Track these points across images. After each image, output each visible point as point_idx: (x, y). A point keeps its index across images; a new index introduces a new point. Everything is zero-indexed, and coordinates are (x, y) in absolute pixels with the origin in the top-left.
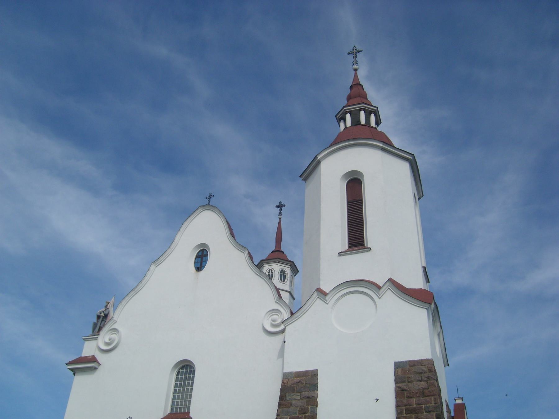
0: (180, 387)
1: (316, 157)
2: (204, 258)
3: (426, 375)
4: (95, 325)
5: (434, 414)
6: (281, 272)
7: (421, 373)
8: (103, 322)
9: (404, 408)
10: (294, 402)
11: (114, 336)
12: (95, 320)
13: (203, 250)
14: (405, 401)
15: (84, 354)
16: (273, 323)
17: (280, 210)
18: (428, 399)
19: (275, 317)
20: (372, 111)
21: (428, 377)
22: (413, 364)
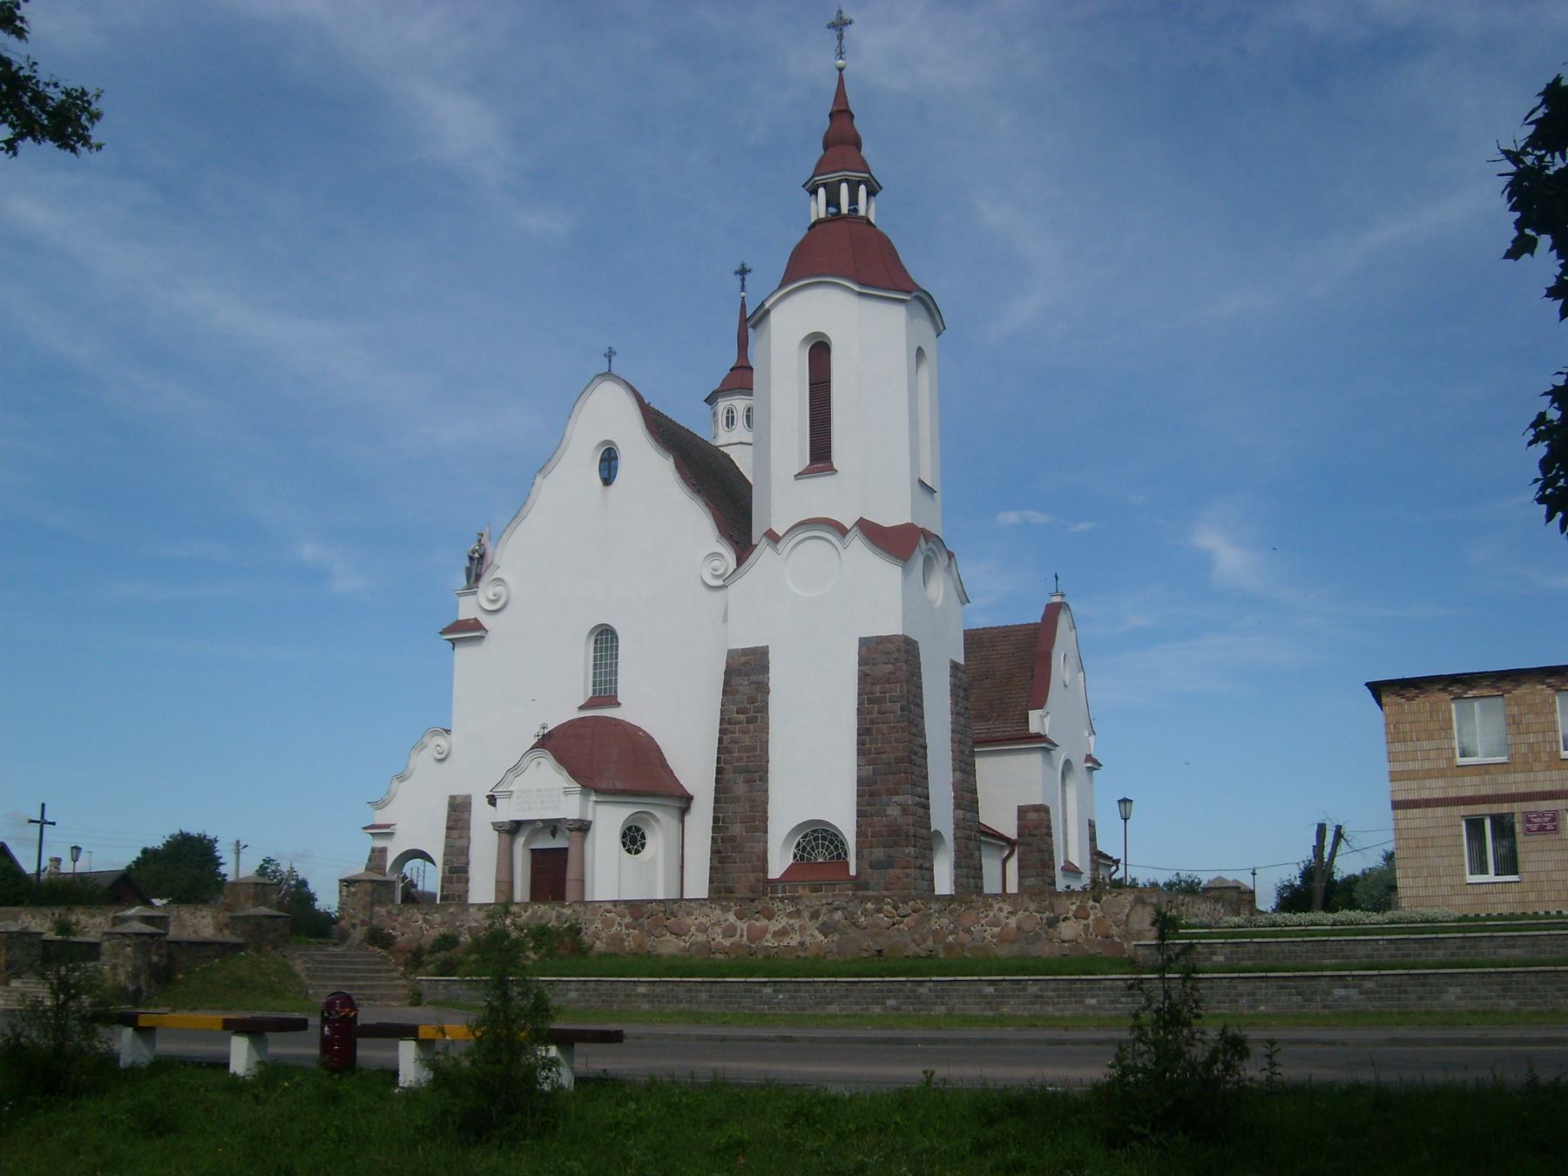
2: (613, 462)
3: (894, 656)
4: (469, 571)
7: (888, 653)
11: (499, 589)
12: (467, 564)
15: (462, 617)
16: (716, 573)
17: (743, 280)
19: (716, 563)
21: (896, 659)
22: (881, 640)
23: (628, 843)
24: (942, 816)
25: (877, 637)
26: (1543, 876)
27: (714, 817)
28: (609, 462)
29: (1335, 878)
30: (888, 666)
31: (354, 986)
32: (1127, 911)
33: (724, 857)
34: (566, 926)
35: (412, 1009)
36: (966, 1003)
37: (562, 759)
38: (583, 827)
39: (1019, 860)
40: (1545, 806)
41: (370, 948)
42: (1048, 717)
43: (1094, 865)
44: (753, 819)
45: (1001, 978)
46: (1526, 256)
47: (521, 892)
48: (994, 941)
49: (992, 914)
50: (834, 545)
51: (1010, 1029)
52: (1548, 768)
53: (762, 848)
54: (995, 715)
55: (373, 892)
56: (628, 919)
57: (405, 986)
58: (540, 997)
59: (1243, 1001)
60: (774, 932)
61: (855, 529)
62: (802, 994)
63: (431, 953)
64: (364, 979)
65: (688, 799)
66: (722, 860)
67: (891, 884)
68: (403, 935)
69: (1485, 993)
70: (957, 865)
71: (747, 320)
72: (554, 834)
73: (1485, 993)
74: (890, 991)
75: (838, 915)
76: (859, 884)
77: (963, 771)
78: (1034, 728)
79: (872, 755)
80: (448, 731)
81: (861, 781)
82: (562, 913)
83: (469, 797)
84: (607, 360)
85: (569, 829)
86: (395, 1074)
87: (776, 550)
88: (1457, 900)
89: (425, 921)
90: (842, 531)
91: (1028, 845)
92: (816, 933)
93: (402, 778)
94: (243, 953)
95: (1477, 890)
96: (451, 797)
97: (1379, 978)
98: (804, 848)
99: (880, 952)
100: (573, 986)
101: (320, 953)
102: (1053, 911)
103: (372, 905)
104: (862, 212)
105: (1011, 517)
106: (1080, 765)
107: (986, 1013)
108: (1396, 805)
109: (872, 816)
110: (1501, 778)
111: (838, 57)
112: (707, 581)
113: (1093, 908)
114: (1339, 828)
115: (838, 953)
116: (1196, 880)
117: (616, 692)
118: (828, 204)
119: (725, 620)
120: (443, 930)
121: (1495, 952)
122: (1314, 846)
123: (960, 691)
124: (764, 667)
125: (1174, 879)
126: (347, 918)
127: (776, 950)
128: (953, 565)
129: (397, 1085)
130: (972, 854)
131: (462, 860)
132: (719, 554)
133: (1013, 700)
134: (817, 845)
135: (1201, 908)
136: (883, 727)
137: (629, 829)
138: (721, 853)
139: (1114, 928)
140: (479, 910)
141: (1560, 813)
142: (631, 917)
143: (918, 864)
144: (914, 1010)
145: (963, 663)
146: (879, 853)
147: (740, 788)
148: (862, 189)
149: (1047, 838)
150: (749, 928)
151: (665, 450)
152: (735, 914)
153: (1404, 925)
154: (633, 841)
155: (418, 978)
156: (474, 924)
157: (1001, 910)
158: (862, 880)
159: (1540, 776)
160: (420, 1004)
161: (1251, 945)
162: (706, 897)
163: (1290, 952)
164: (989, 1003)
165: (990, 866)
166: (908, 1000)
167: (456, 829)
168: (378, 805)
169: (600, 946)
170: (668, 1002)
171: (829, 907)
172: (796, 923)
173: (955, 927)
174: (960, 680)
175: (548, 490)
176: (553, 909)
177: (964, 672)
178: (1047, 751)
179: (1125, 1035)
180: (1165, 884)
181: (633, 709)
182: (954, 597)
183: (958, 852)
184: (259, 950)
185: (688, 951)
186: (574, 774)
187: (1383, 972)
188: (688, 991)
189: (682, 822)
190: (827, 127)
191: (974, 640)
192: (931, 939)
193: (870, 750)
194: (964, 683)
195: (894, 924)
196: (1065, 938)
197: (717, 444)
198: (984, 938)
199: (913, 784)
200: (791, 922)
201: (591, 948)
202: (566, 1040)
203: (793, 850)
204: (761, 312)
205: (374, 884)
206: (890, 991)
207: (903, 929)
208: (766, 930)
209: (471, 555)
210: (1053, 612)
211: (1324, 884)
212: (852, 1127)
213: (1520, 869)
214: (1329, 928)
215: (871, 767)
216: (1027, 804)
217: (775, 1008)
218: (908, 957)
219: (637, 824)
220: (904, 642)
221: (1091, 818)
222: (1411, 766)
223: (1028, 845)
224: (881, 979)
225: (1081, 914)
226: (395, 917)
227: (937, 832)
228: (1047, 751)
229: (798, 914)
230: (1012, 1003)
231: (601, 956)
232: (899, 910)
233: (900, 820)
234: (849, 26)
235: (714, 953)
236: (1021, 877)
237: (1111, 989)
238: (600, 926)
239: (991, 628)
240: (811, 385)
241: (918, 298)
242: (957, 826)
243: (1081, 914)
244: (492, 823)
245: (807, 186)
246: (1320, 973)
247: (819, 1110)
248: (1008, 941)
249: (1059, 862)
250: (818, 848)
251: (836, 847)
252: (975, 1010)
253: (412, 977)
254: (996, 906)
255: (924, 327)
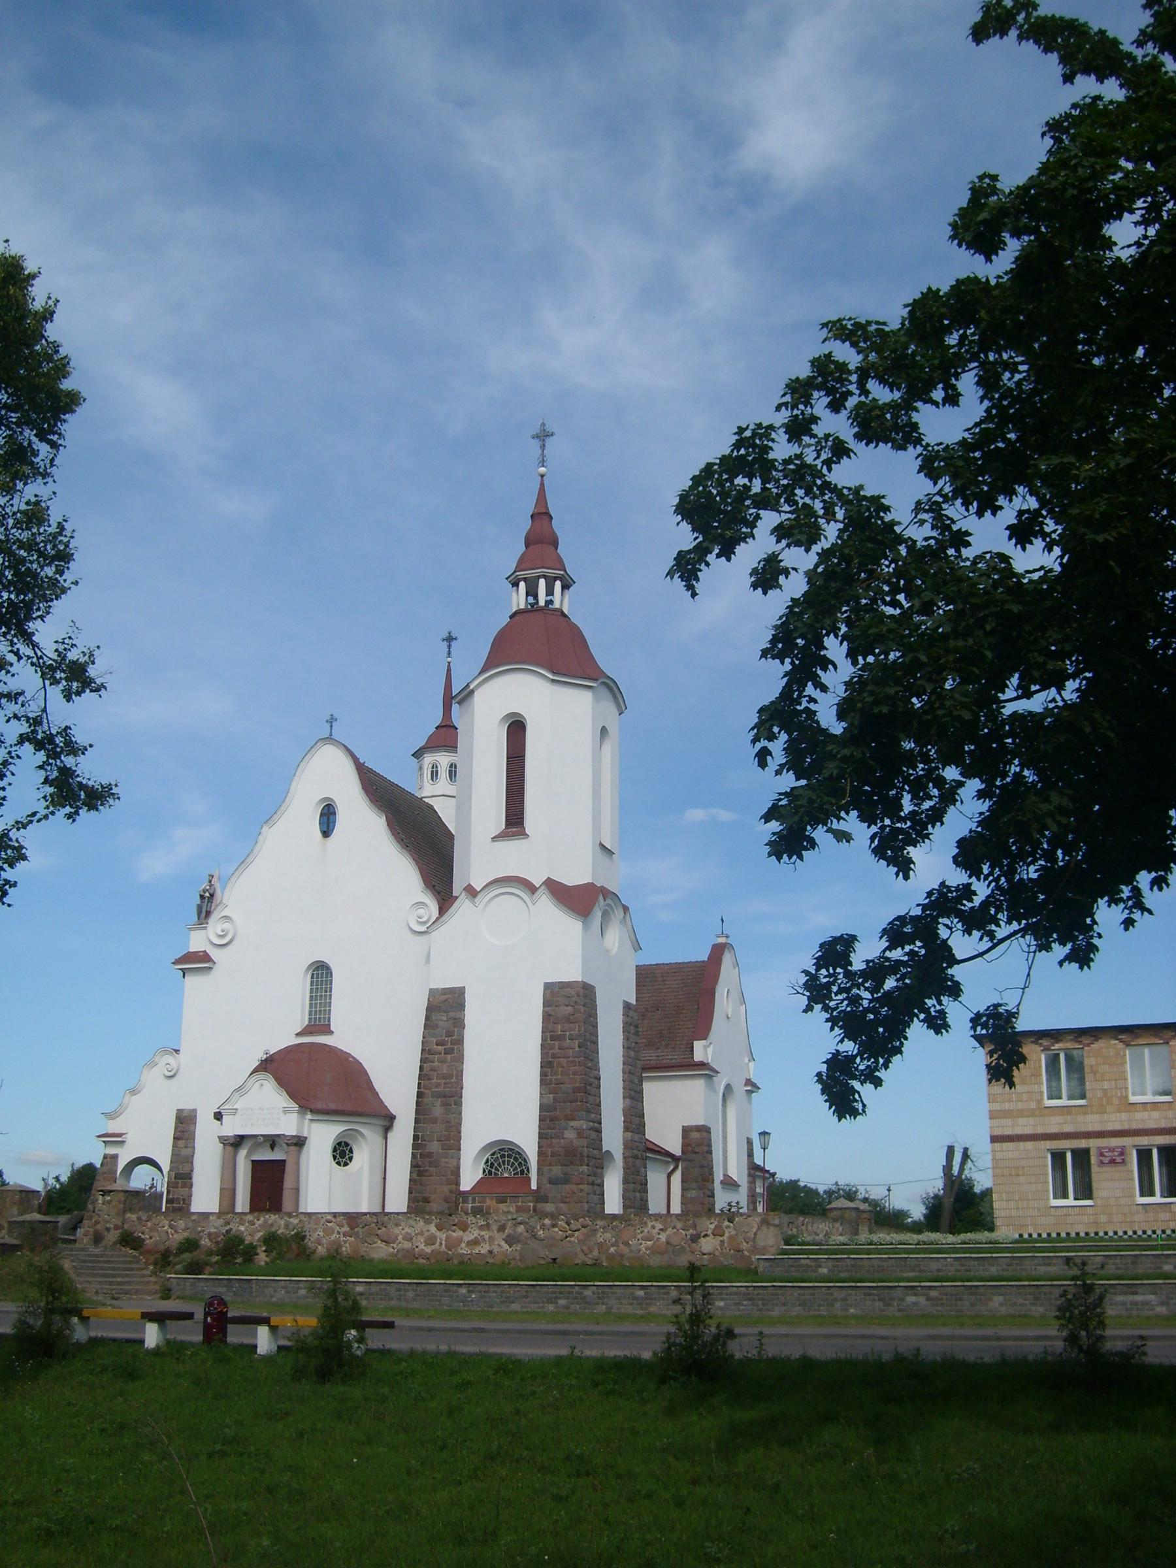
0: (317, 992)
1: (468, 685)
2: (331, 817)
3: (574, 999)
4: (200, 908)
5: (577, 1042)
6: (451, 766)
8: (210, 904)
9: (548, 1034)
10: (441, 1023)
11: (227, 926)
12: (198, 901)
13: (328, 805)
14: (550, 1026)
16: (421, 920)
18: (572, 1025)
19: (421, 911)
20: (555, 577)
21: (575, 1002)
23: (338, 1156)
24: (613, 1137)
25: (559, 982)
26: (1112, 1202)
27: (414, 1135)
28: (328, 817)
29: (975, 1191)
30: (569, 1008)
31: (113, 1282)
32: (754, 1230)
33: (422, 1171)
34: (293, 1233)
35: (164, 1302)
36: (621, 1304)
37: (283, 1082)
38: (299, 1142)
39: (682, 1175)
40: (1115, 1142)
41: (123, 1249)
42: (712, 1046)
43: (751, 1179)
44: (448, 1138)
45: (650, 1284)
46: (810, 1012)
47: (242, 1202)
48: (648, 1252)
49: (646, 1231)
50: (525, 902)
51: (653, 1324)
52: (1119, 1111)
53: (455, 1164)
54: (664, 1043)
55: (125, 1201)
56: (346, 1229)
57: (155, 1283)
58: (355, 1302)
59: (838, 1305)
60: (468, 1242)
61: (543, 887)
62: (491, 1294)
63: (177, 1255)
64: (120, 1276)
65: (392, 1118)
66: (420, 1174)
67: (566, 1197)
68: (151, 1238)
69: (1020, 1301)
70: (625, 1181)
71: (453, 698)
72: (272, 1147)
73: (1020, 1301)
74: (561, 1293)
75: (521, 1229)
76: (540, 1197)
77: (632, 1098)
78: (698, 1056)
79: (554, 1085)
80: (177, 1051)
81: (543, 1108)
82: (290, 1223)
83: (195, 1111)
84: (328, 725)
85: (287, 1144)
86: (256, 1347)
87: (473, 903)
88: (1042, 1220)
89: (171, 1226)
90: (532, 889)
91: (691, 1161)
92: (503, 1243)
93: (134, 1092)
94: (19, 1253)
95: (1059, 1212)
96: (178, 1110)
97: (942, 1289)
98: (492, 1164)
99: (554, 1260)
100: (302, 1285)
101: (83, 1253)
102: (696, 1229)
103: (125, 1211)
104: (557, 605)
105: (697, 815)
106: (740, 1088)
107: (637, 1312)
108: (995, 1139)
109: (551, 1138)
110: (1080, 1118)
111: (541, 464)
112: (415, 929)
113: (728, 1227)
114: (966, 1150)
115: (520, 1260)
116: (854, 1189)
117: (329, 1021)
118: (528, 594)
119: (428, 961)
120: (186, 1234)
121: (1035, 1269)
122: (944, 1166)
123: (632, 1027)
124: (461, 1005)
125: (834, 1188)
126: (102, 1222)
127: (469, 1256)
128: (628, 918)
129: (256, 1353)
130: (639, 1171)
131: (186, 1170)
132: (423, 904)
133: (680, 1031)
134: (504, 1162)
135: (820, 1227)
136: (563, 1061)
137: (339, 1144)
138: (420, 1167)
139: (744, 1244)
140: (219, 1218)
141: (1128, 1148)
142: (349, 1227)
143: (590, 1181)
144: (580, 1308)
145: (635, 1003)
146: (557, 1171)
147: (438, 1111)
148: (558, 584)
149: (708, 1155)
150: (447, 1238)
151: (379, 809)
152: (436, 1226)
153: (972, 1246)
154: (343, 1155)
155: (169, 1276)
156: (213, 1230)
157: (653, 1227)
158: (542, 1194)
159: (1113, 1117)
160: (169, 1298)
161: (848, 1261)
162: (405, 1211)
163: (879, 1267)
164: (640, 1304)
165: (655, 1179)
166: (576, 1300)
167: (182, 1139)
168: (111, 1116)
169: (321, 1250)
170: (381, 1299)
171: (514, 1222)
172: (486, 1234)
173: (616, 1240)
174: (632, 1018)
175: (273, 838)
176: (282, 1218)
177: (636, 1011)
178: (710, 1077)
179: (672, 1329)
180: (825, 1192)
181: (343, 1037)
182: (628, 946)
183: (626, 1169)
184: (32, 1250)
185: (396, 1256)
186: (292, 1095)
187: (944, 1284)
188: (399, 1290)
189: (386, 1138)
190: (529, 527)
191: (646, 976)
192: (596, 1249)
193: (551, 1080)
194: (634, 1019)
195: (567, 1237)
196: (705, 1252)
197: (423, 795)
198: (640, 1250)
199: (588, 1112)
200: (483, 1233)
201: (314, 1252)
202: (362, 1326)
203: (482, 1165)
204: (466, 692)
205: (127, 1194)
206: (561, 1293)
207: (574, 1242)
208: (460, 1240)
209: (202, 893)
210: (718, 952)
211: (952, 1200)
212: (529, 1375)
213: (1095, 1195)
214: (914, 1246)
215: (551, 1095)
216: (690, 1124)
217: (468, 1305)
218: (577, 1264)
219: (344, 1140)
220: (583, 988)
221: (750, 1137)
222: (1007, 1106)
223: (691, 1161)
224: (554, 1283)
225: (718, 1232)
226: (144, 1223)
227: (608, 1152)
228: (710, 1077)
229: (488, 1227)
230: (658, 1304)
231: (322, 1259)
232: (571, 1226)
233: (577, 1143)
234: (551, 438)
235: (417, 1258)
236: (684, 1189)
237: (735, 1294)
238: (321, 1234)
239: (663, 964)
240: (508, 758)
241: (604, 683)
242: (626, 1146)
243: (718, 1232)
244: (218, 1137)
245: (509, 580)
246: (896, 1284)
247: (511, 1366)
248: (659, 1253)
249: (718, 1176)
250: (504, 1164)
251: (520, 1164)
252: (629, 1309)
253: (162, 1274)
254: (650, 1224)
255: (609, 707)
